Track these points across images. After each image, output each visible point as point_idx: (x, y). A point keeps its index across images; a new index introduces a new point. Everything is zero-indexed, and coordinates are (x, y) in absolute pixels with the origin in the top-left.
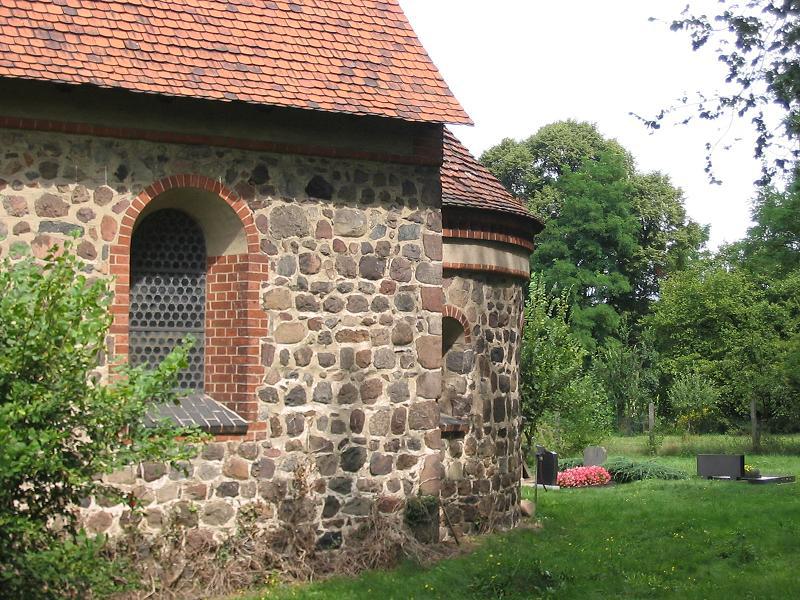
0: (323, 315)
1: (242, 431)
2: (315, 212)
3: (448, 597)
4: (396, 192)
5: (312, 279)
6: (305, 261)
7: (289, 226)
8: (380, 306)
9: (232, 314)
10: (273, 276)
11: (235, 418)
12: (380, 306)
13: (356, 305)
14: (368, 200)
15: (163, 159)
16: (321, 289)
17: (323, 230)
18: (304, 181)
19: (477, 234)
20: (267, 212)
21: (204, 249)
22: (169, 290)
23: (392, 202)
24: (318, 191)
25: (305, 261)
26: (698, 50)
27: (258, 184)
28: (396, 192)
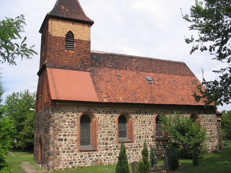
0: (206, 126)
1: (132, 142)
2: (205, 115)
3: (141, 172)
4: (212, 113)
5: (205, 122)
6: (205, 120)
7: (203, 117)
8: (211, 125)
9: (94, 130)
10: (202, 122)
11: (131, 141)
12: (211, 125)
13: (209, 125)
14: (209, 114)
15: (192, 111)
16: (206, 123)
17: (206, 117)
18: (204, 112)
19: (219, 117)
20: (201, 116)
21: (90, 119)
22: (122, 125)
23: (212, 114)
24: (205, 113)
25: (205, 120)
26: (13, 16)
27: (200, 113)
28: (212, 113)
